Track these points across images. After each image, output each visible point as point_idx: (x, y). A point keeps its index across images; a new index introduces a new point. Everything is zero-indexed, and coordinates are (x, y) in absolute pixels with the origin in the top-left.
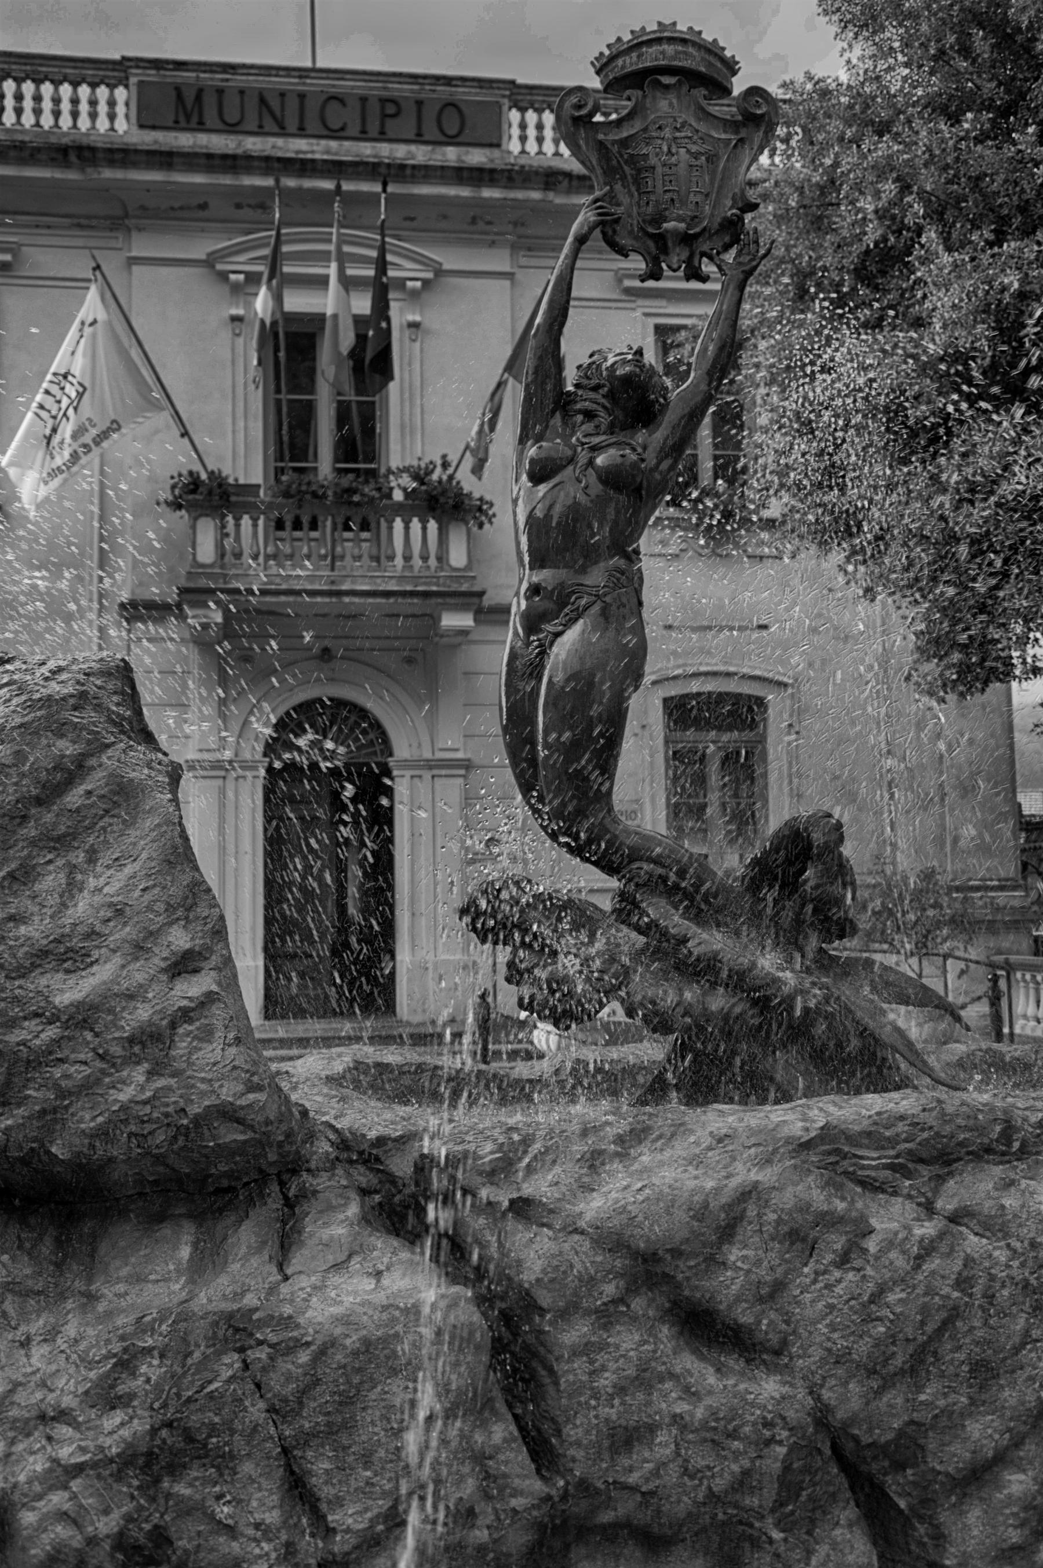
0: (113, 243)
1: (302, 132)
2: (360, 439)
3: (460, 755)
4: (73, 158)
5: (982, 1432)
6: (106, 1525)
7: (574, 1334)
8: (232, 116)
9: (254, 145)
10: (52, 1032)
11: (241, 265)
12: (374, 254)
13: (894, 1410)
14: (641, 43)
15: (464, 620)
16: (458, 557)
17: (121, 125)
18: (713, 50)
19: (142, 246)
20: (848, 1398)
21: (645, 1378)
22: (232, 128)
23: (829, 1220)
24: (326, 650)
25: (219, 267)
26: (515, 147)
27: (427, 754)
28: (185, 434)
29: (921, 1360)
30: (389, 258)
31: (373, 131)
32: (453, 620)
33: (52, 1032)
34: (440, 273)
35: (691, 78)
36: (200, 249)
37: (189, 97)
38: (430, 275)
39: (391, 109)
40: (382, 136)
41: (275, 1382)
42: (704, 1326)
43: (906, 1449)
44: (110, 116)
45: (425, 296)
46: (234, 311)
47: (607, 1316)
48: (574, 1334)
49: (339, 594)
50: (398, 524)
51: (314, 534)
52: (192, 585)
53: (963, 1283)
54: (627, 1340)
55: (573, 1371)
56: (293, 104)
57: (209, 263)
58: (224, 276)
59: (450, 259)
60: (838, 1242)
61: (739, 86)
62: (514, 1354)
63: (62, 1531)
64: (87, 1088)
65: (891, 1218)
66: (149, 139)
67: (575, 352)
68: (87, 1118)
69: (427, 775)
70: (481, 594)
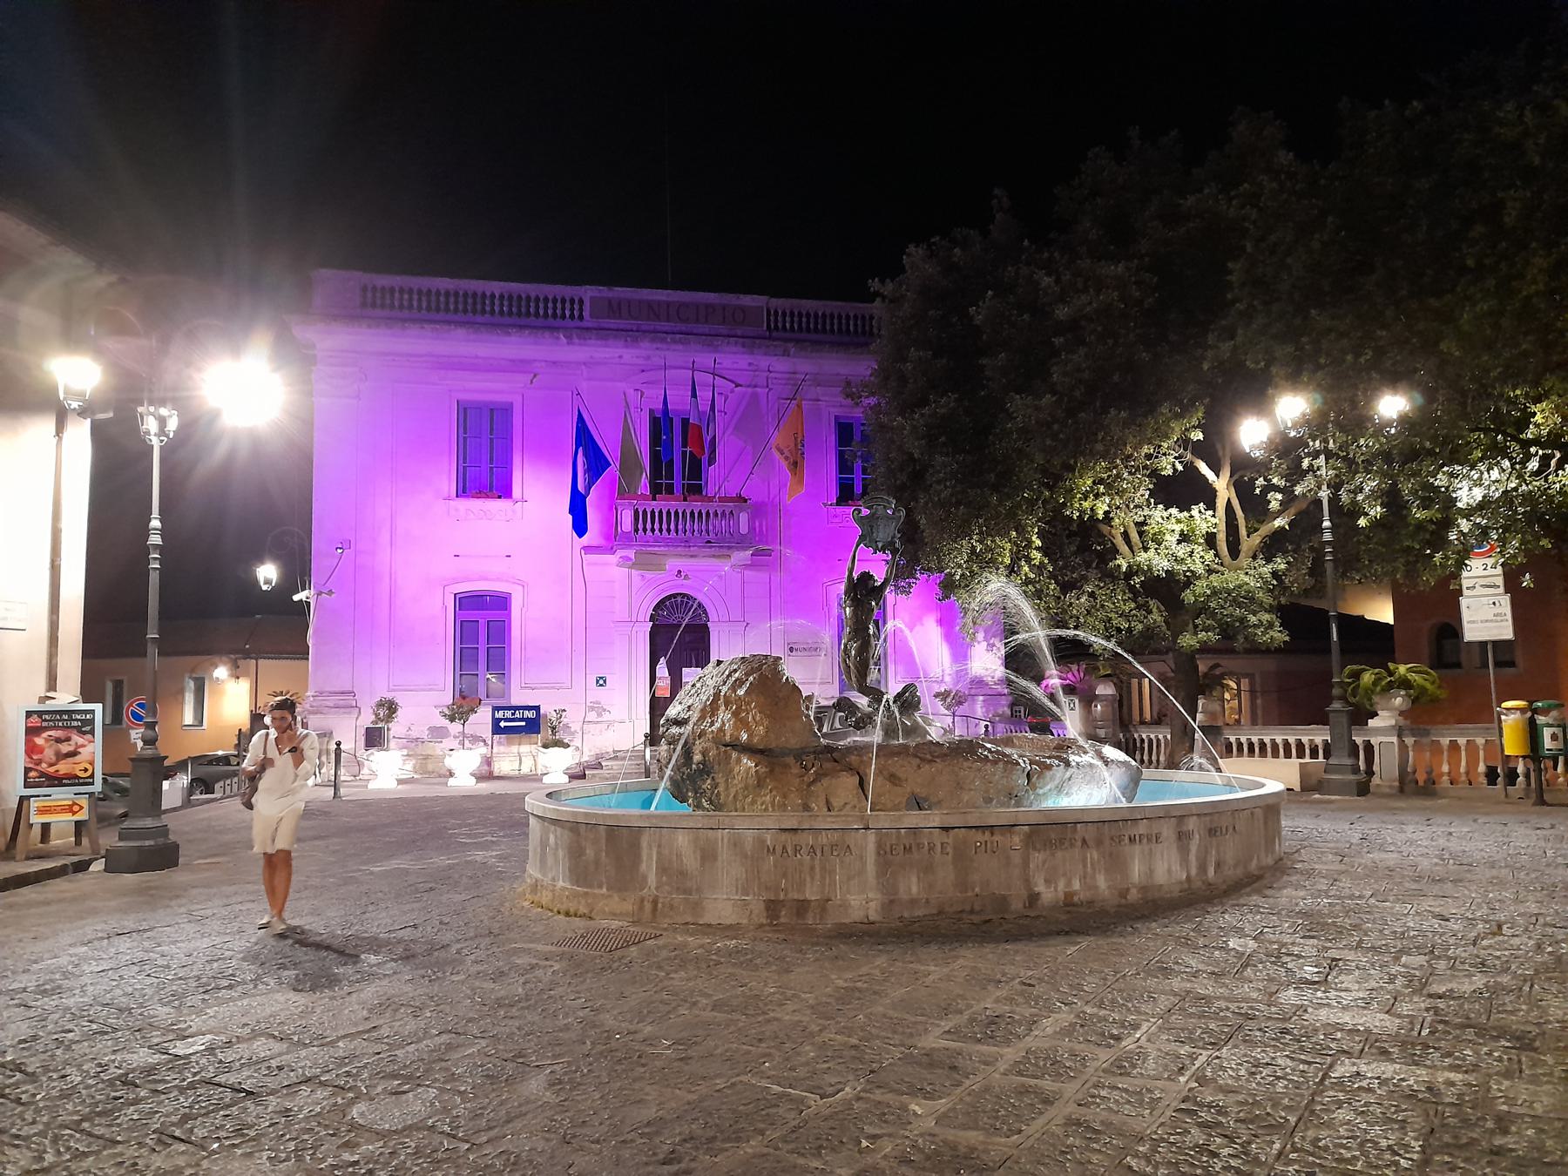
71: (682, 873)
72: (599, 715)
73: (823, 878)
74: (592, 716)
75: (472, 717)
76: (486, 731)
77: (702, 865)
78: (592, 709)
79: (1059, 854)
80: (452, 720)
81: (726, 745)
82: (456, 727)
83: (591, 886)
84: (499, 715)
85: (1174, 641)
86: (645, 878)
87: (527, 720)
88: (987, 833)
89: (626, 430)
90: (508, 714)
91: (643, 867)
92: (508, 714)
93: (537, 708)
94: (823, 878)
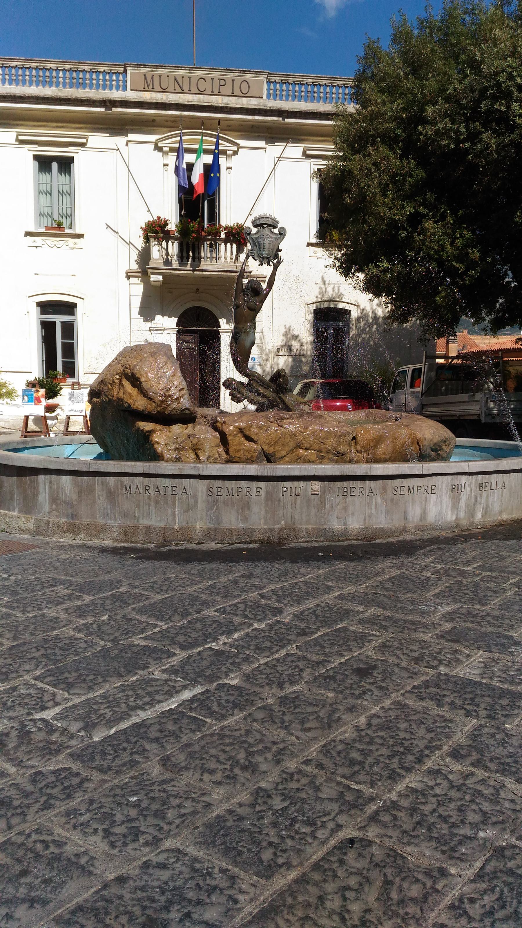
1: (190, 92)
5: (283, 453)
11: (167, 144)
12: (215, 140)
14: (260, 218)
18: (274, 220)
19: (132, 137)
20: (266, 448)
21: (240, 444)
22: (164, 91)
24: (198, 289)
28: (149, 211)
29: (276, 443)
30: (220, 141)
31: (216, 92)
35: (269, 226)
36: (153, 138)
37: (149, 78)
38: (236, 149)
39: (222, 83)
40: (219, 94)
42: (249, 439)
43: (273, 454)
50: (223, 245)
54: (237, 439)
56: (186, 80)
59: (243, 143)
61: (279, 226)
77: (80, 497)
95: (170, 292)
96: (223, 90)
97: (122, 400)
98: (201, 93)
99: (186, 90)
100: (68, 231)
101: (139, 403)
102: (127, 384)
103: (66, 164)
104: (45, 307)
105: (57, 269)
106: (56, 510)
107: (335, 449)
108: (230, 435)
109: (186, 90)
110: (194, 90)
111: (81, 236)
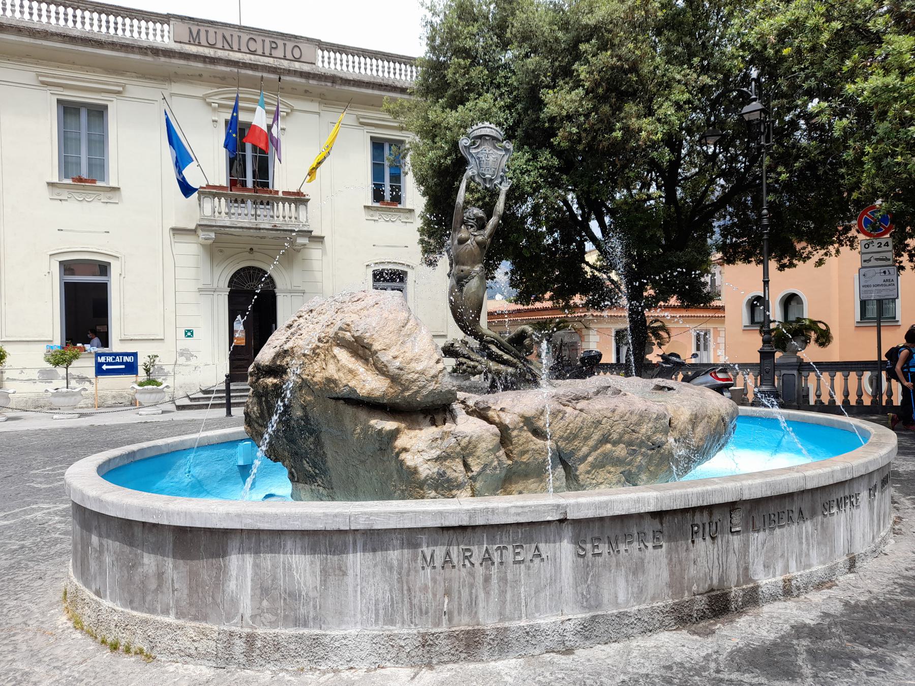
0: (163, 86)
1: (239, 51)
2: (263, 170)
3: (301, 288)
4: (149, 52)
6: (436, 470)
7: (515, 433)
8: (212, 41)
9: (221, 54)
10: (417, 375)
13: (570, 447)
15: (305, 241)
16: (302, 218)
17: (166, 39)
23: (559, 411)
24: (251, 249)
25: (208, 100)
26: (320, 64)
27: (289, 288)
31: (267, 53)
32: (301, 241)
33: (417, 375)
34: (292, 110)
39: (274, 45)
40: (271, 56)
41: (463, 444)
43: (572, 453)
44: (162, 37)
45: (288, 118)
46: (214, 118)
47: (521, 429)
48: (515, 433)
49: (260, 229)
51: (243, 205)
52: (202, 223)
53: (583, 422)
55: (515, 440)
57: (204, 98)
58: (209, 104)
60: (561, 415)
62: (505, 437)
63: (428, 471)
64: (424, 387)
65: (569, 410)
66: (177, 47)
67: (678, 303)
68: (425, 392)
69: (289, 295)
70: (311, 232)
71: (291, 595)
72: (188, 359)
73: (503, 593)
74: (182, 360)
75: (75, 363)
76: (91, 372)
77: (324, 582)
78: (182, 355)
79: (778, 531)
80: (57, 364)
81: (337, 399)
82: (61, 371)
83: (152, 611)
84: (102, 359)
85: (643, 308)
86: (234, 602)
87: (126, 364)
88: (705, 514)
89: (168, 121)
90: (110, 359)
91: (232, 585)
92: (110, 359)
93: (135, 355)
94: (503, 593)
95: (221, 251)
96: (275, 53)
97: (334, 382)
98: (253, 53)
99: (236, 48)
100: (99, 184)
101: (370, 383)
102: (343, 355)
103: (99, 113)
104: (68, 267)
105: (84, 227)
106: (269, 611)
107: (649, 438)
108: (515, 428)
109: (235, 48)
110: (244, 49)
111: (116, 189)
